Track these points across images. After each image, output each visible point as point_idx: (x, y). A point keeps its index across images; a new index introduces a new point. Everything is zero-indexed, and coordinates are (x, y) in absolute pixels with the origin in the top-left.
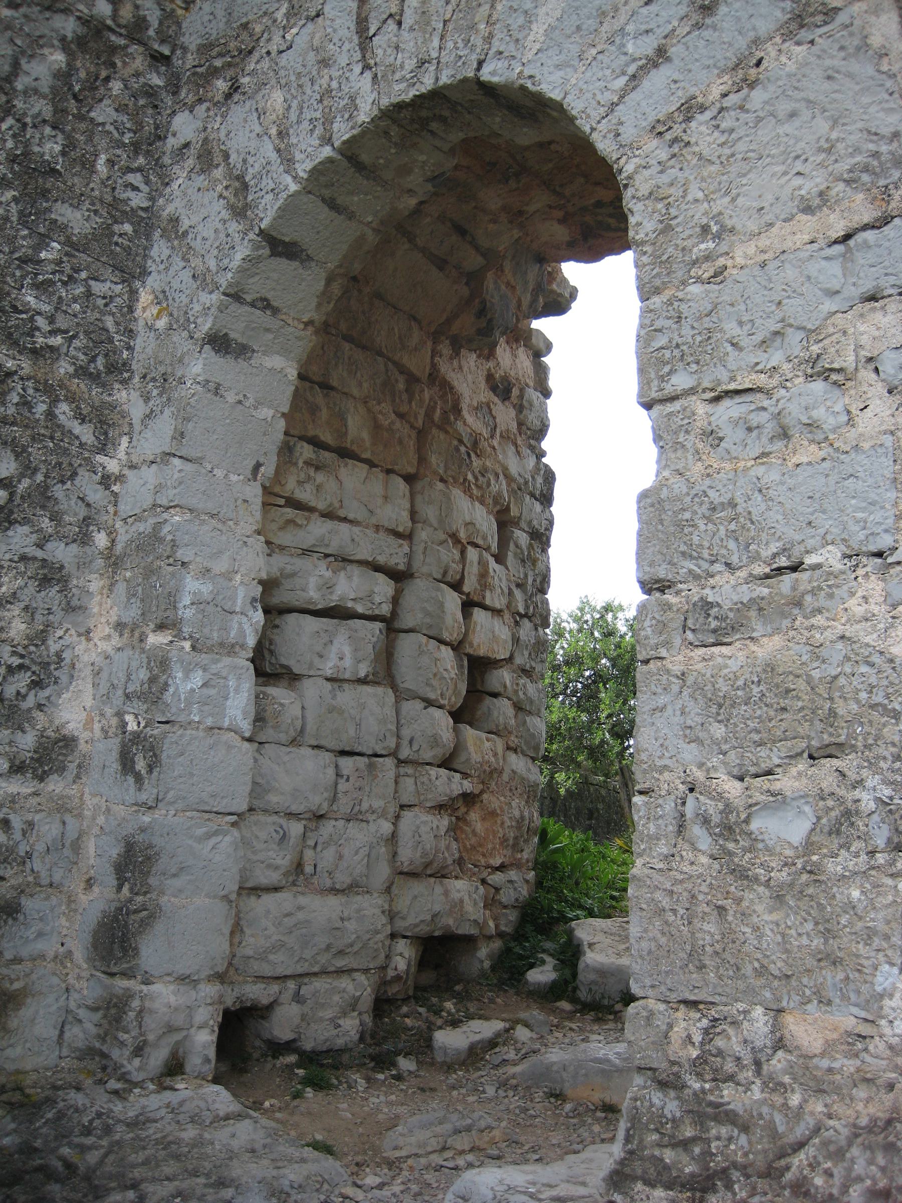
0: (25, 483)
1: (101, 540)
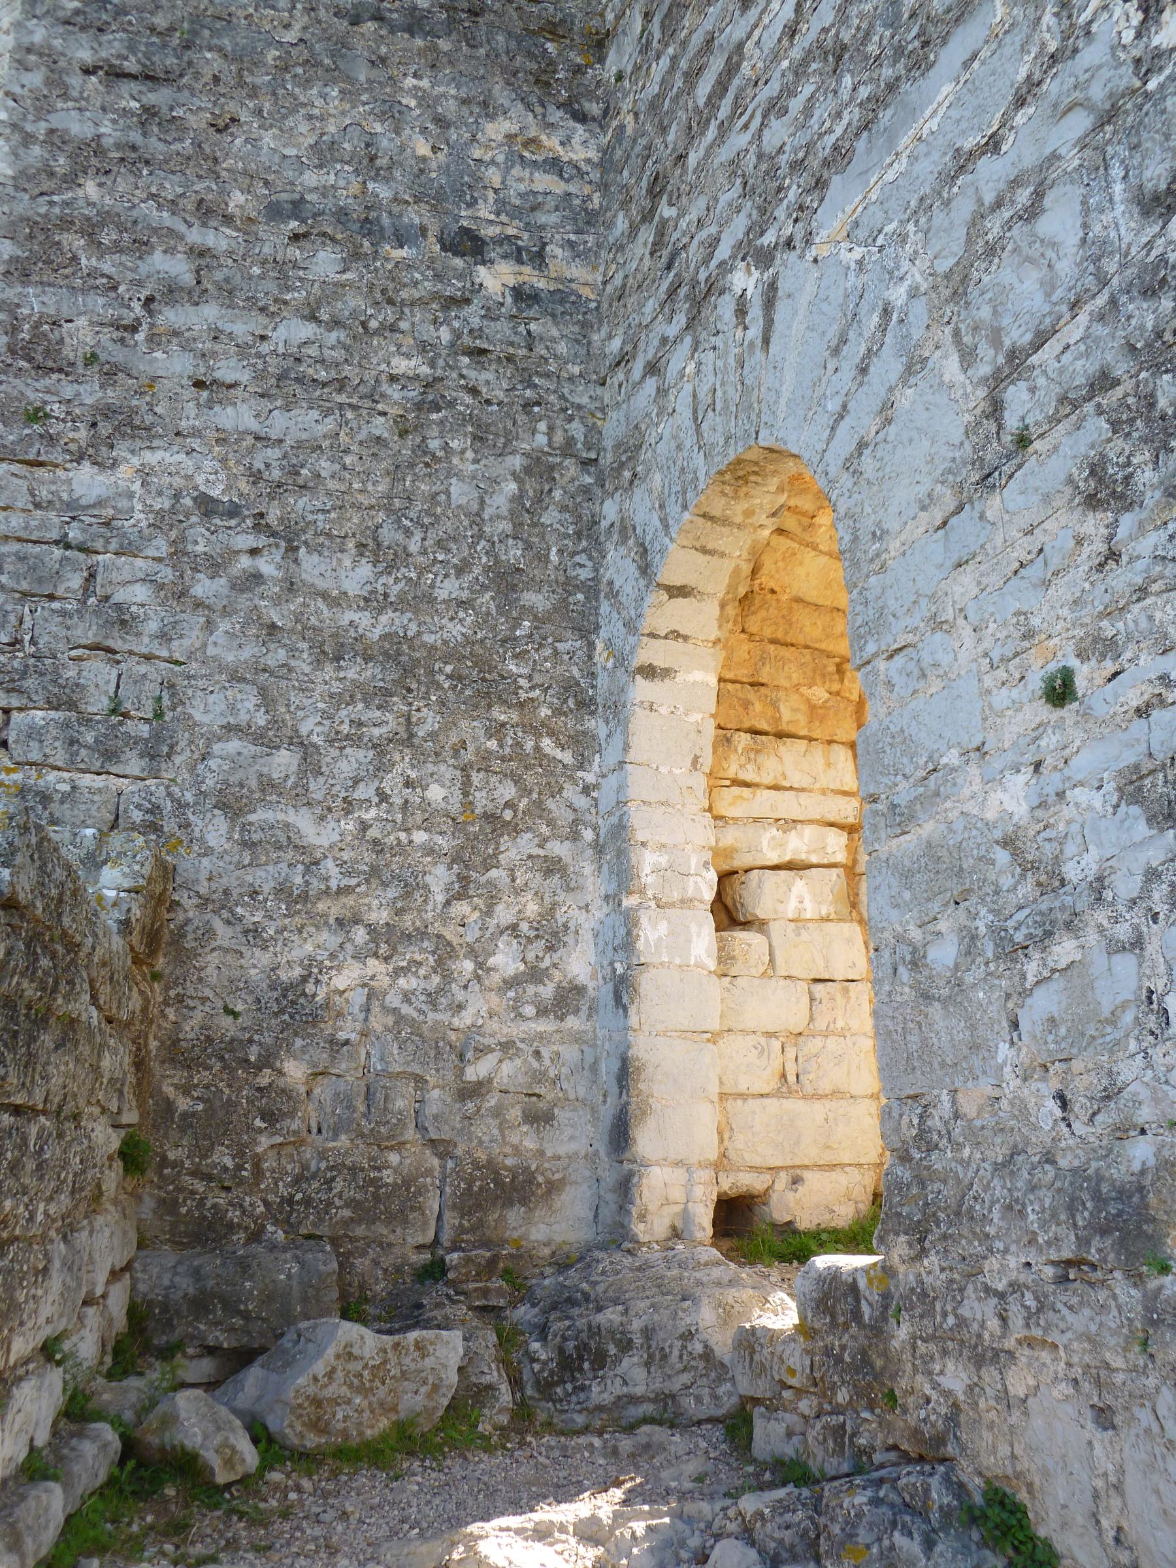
1: (588, 835)
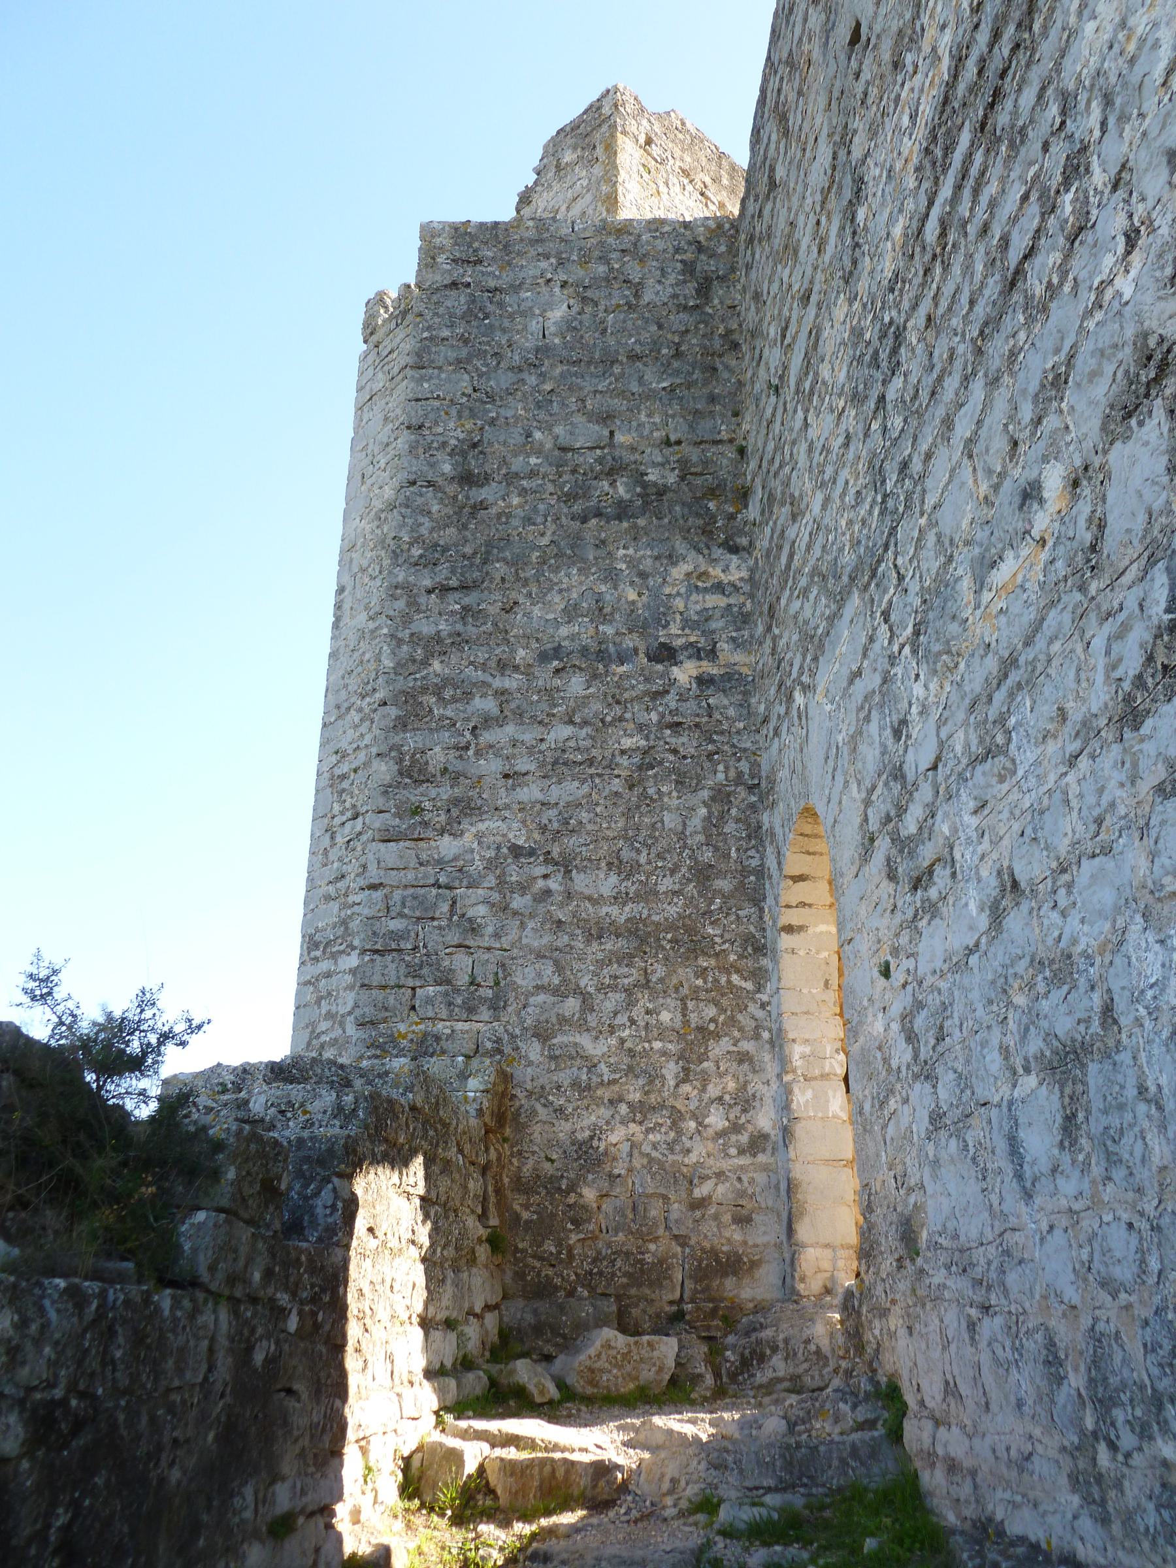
0: (722, 1018)
1: (766, 1035)
